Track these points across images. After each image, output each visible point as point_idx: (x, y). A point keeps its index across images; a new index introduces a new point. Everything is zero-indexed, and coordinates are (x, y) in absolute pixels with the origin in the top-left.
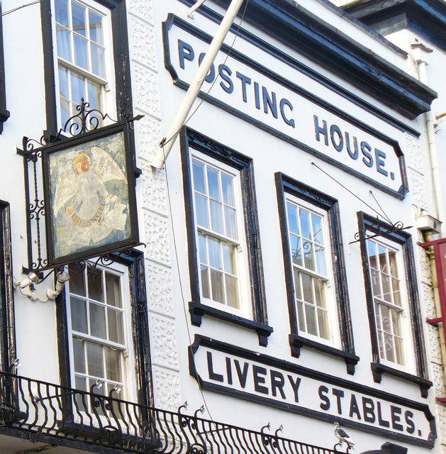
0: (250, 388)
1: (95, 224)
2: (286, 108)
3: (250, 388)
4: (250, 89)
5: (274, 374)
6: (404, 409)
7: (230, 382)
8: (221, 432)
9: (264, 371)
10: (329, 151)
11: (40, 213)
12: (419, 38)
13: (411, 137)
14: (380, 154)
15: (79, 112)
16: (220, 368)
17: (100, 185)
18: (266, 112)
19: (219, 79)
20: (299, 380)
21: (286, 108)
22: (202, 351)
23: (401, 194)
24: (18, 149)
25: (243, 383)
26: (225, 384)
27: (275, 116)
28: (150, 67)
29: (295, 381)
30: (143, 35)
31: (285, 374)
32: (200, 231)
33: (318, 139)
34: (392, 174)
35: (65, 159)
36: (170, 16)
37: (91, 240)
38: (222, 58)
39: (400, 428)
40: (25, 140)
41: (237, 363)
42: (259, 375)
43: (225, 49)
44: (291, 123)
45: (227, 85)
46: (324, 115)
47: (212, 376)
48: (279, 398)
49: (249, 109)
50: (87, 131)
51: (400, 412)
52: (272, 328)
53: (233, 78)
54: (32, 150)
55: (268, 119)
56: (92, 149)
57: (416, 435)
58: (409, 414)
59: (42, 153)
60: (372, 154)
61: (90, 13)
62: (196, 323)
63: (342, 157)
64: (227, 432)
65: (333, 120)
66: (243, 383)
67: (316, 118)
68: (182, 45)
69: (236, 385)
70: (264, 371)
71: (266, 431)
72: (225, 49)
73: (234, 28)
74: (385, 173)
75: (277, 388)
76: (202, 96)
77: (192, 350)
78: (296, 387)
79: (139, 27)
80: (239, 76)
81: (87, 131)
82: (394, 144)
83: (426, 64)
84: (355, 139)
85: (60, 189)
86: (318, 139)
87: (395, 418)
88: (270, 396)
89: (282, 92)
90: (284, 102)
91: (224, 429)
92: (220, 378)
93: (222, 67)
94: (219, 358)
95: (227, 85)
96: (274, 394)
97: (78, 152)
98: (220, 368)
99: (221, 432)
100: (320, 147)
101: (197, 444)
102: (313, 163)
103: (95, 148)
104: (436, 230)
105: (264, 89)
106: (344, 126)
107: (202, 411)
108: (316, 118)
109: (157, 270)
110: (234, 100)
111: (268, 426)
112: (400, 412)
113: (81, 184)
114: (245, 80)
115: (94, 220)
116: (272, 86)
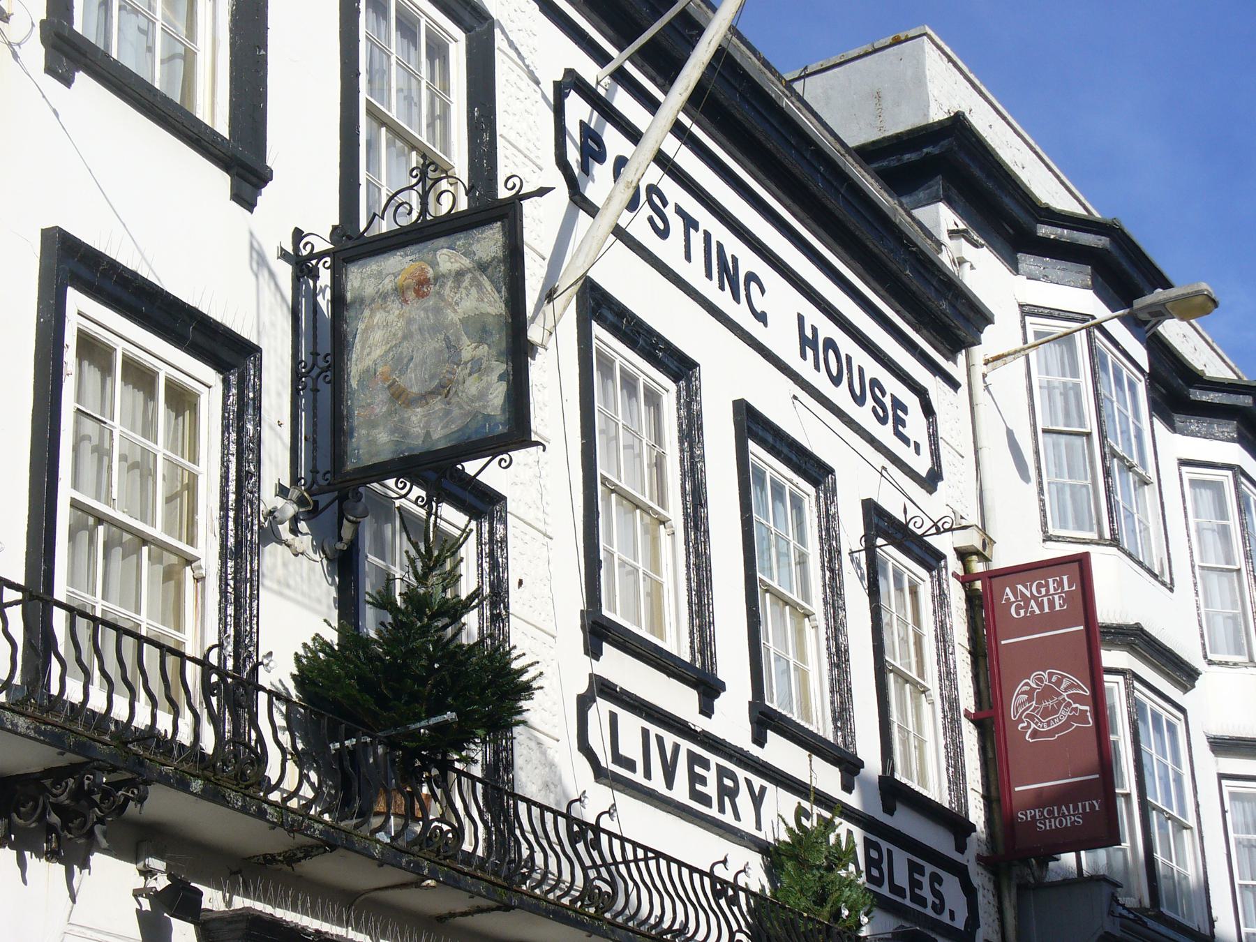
0: (680, 792)
1: (437, 404)
2: (754, 287)
3: (680, 792)
4: (697, 239)
5: (722, 772)
6: (929, 868)
7: (648, 774)
8: (642, 864)
9: (705, 764)
10: (820, 381)
11: (322, 376)
12: (959, 222)
13: (947, 388)
14: (897, 404)
15: (414, 181)
16: (631, 747)
17: (452, 324)
18: (722, 288)
19: (645, 211)
20: (763, 789)
21: (754, 287)
22: (601, 709)
23: (931, 481)
24: (282, 249)
25: (670, 781)
26: (638, 777)
27: (736, 297)
28: (532, 156)
29: (757, 790)
30: (521, 95)
31: (741, 774)
32: (604, 479)
33: (803, 356)
34: (917, 446)
35: (380, 272)
36: (570, 73)
37: (428, 434)
38: (654, 174)
39: (922, 901)
40: (298, 235)
41: (660, 740)
42: (698, 770)
43: (662, 160)
44: (762, 317)
45: (661, 225)
46: (814, 317)
47: (618, 759)
48: (728, 818)
49: (693, 273)
50: (429, 218)
51: (923, 875)
52: (723, 683)
53: (669, 211)
54: (312, 256)
55: (723, 300)
56: (438, 253)
57: (945, 918)
58: (935, 879)
59: (333, 262)
60: (887, 401)
61: (427, 29)
62: (594, 651)
63: (840, 396)
64: (652, 864)
65: (828, 329)
66: (670, 781)
67: (801, 319)
68: (587, 132)
69: (657, 783)
70: (705, 764)
71: (719, 871)
72: (662, 160)
73: (678, 130)
74: (906, 440)
75: (727, 799)
76: (620, 233)
77: (584, 703)
78: (757, 800)
79: (513, 77)
80: (679, 211)
81: (429, 218)
82: (920, 392)
83: (972, 267)
84: (861, 370)
85: (366, 330)
86: (803, 356)
87: (915, 884)
88: (713, 812)
89: (749, 261)
90: (751, 277)
91: (646, 859)
92: (630, 765)
93: (652, 189)
94: (631, 724)
95: (661, 225)
96: (722, 809)
97: (409, 258)
98: (631, 747)
99: (642, 864)
100: (805, 368)
101: (600, 877)
102: (795, 397)
103: (445, 251)
104: (986, 553)
105: (720, 246)
106: (846, 345)
107: (611, 815)
108: (801, 319)
109: (527, 538)
110: (669, 250)
111: (725, 862)
112: (923, 875)
113: (410, 322)
114: (690, 223)
115: (434, 393)
116: (734, 246)
